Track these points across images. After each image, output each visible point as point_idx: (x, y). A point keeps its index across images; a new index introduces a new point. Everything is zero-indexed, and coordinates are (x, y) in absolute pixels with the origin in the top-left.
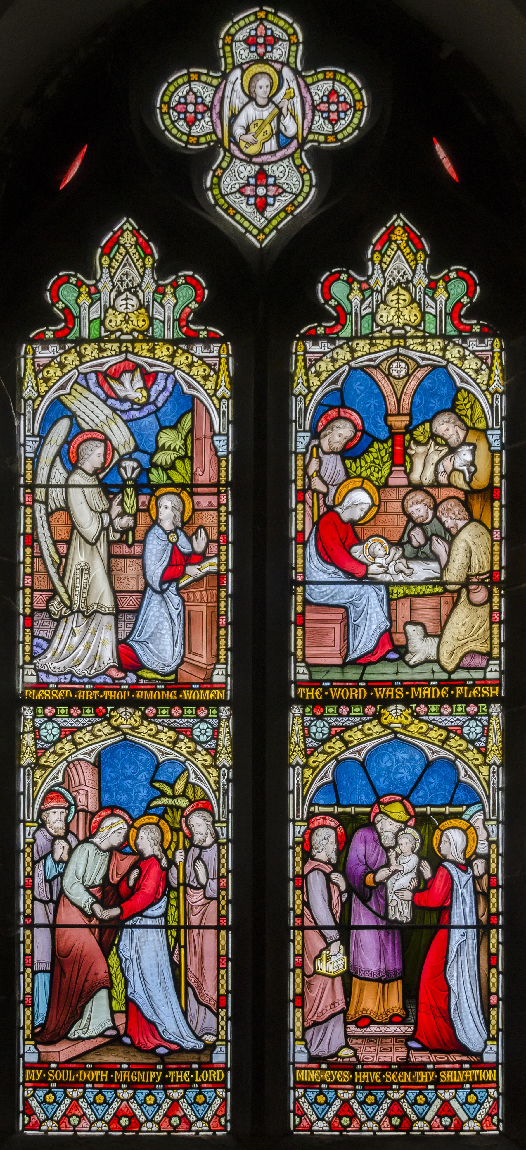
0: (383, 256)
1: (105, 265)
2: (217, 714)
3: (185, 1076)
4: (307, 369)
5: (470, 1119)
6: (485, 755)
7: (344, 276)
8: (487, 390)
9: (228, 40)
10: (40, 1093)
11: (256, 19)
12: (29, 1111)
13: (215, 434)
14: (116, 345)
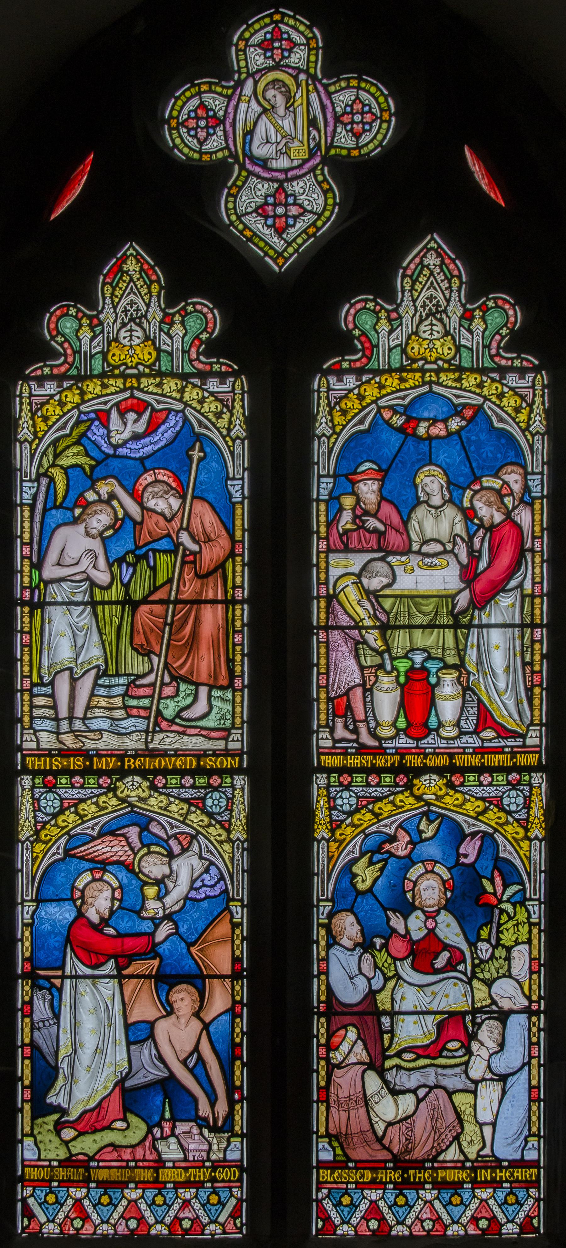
0: (114, 289)
1: (407, 288)
2: (232, 783)
3: (427, 1175)
4: (34, 414)
5: (508, 1221)
6: (229, 831)
7: (491, 304)
8: (228, 435)
9: (242, 45)
10: (150, 1194)
11: (272, 22)
12: (28, 1213)
13: (228, 478)
14: (120, 382)
